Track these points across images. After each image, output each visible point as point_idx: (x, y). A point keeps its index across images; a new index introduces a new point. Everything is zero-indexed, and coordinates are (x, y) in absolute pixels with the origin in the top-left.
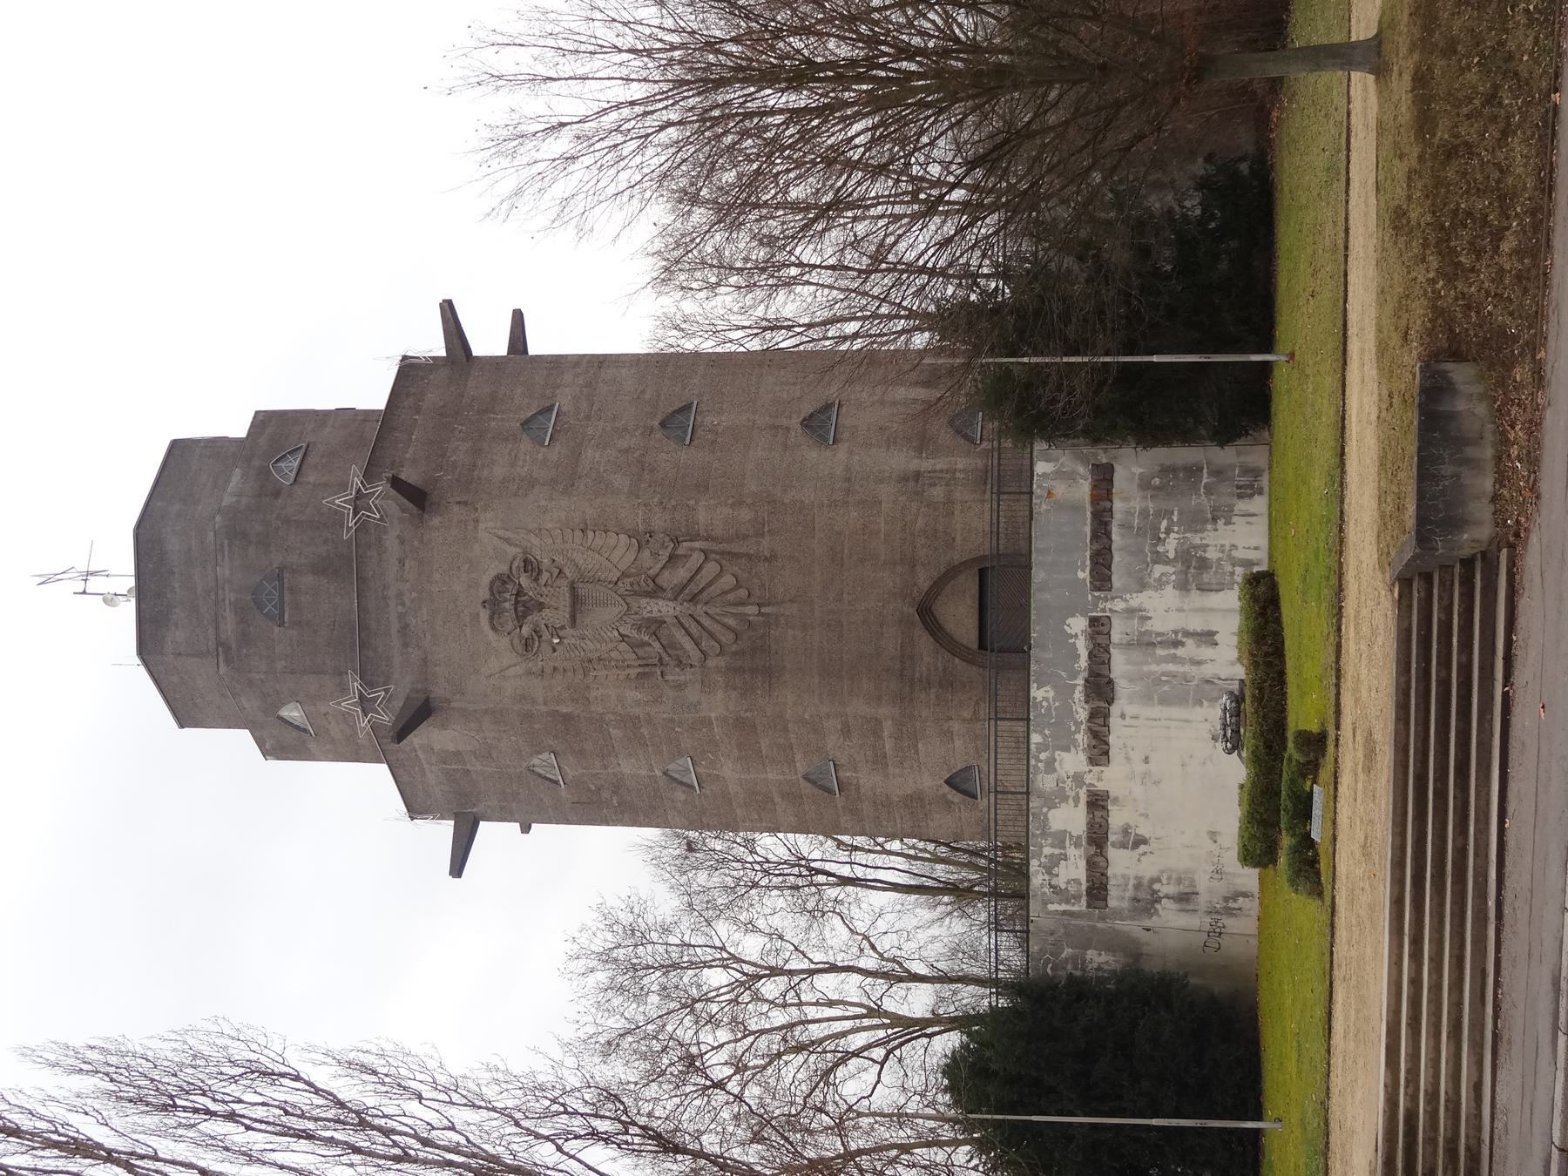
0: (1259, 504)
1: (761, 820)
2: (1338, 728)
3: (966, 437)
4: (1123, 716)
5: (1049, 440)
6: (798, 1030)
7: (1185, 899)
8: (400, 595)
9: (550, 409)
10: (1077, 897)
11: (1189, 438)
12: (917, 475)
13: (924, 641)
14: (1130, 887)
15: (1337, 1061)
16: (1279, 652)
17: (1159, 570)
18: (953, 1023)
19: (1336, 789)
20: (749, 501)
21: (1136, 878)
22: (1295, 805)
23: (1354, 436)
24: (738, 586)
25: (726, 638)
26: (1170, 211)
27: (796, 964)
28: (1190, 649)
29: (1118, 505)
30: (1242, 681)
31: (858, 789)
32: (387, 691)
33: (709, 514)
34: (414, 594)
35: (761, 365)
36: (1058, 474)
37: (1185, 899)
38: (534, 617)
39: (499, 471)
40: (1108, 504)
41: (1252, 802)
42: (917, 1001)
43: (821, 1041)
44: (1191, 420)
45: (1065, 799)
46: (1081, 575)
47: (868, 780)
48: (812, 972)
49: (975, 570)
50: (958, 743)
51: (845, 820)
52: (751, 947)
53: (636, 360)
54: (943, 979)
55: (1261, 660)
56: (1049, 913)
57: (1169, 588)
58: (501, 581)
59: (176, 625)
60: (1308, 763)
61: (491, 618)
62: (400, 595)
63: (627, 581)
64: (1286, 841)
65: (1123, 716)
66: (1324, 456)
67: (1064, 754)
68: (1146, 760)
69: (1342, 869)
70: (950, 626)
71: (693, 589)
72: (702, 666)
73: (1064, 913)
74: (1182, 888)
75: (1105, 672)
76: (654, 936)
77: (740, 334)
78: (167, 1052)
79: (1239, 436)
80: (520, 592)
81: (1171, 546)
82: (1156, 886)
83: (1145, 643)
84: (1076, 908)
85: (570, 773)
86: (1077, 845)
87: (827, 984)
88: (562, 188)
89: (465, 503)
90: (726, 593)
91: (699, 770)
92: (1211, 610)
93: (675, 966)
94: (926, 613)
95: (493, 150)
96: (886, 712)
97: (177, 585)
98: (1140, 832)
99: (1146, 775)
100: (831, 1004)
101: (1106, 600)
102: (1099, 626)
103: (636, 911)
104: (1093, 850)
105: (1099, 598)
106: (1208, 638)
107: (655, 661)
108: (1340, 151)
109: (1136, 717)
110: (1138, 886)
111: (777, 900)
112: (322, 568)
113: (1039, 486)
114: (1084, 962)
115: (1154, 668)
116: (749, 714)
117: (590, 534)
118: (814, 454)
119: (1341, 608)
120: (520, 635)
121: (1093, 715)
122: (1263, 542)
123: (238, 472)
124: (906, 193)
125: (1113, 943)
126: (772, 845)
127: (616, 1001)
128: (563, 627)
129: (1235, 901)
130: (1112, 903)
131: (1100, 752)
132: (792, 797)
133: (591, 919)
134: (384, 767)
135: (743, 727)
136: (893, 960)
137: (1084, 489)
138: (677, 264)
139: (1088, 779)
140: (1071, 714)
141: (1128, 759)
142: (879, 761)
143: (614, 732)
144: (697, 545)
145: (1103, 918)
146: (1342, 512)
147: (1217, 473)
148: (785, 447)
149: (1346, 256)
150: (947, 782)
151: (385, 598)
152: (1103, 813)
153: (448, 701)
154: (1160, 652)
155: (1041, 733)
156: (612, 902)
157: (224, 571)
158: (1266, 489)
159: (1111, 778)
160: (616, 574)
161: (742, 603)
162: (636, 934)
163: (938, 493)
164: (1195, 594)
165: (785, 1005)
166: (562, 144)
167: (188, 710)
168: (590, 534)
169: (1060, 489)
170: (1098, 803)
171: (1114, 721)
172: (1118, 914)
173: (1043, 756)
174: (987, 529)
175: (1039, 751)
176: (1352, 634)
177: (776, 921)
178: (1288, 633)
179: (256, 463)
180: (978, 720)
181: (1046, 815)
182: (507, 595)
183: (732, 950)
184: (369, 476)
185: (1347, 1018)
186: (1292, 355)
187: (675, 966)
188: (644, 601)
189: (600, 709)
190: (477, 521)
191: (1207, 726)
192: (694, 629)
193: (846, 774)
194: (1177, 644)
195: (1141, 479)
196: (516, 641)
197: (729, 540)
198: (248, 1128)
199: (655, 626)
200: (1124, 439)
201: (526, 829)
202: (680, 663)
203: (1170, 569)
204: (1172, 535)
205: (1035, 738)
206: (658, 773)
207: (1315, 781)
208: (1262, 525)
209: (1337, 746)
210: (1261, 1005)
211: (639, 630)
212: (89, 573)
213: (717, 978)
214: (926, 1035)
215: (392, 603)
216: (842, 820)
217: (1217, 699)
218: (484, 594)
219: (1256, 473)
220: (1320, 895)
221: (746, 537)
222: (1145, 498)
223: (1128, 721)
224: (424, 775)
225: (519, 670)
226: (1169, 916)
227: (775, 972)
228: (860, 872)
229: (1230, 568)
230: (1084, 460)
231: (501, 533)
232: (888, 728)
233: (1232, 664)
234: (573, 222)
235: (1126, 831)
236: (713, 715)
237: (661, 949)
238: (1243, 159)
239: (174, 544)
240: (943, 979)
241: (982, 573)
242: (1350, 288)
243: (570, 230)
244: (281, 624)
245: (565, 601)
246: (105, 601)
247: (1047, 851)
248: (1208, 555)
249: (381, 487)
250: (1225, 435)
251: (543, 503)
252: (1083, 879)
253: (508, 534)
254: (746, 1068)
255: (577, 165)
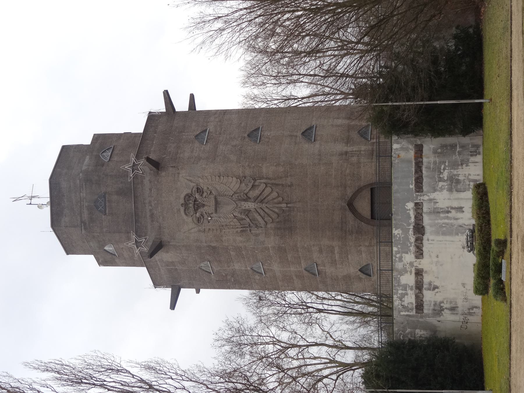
0: (479, 158)
1: (288, 286)
2: (511, 237)
3: (364, 138)
4: (428, 240)
5: (398, 135)
6: (303, 368)
7: (453, 309)
8: (150, 202)
9: (206, 131)
10: (412, 309)
11: (451, 133)
12: (346, 153)
13: (350, 216)
14: (432, 305)
15: (513, 362)
16: (488, 213)
17: (441, 184)
18: (361, 365)
19: (511, 260)
20: (282, 164)
21: (434, 301)
22: (495, 268)
23: (515, 126)
24: (278, 196)
25: (274, 216)
26: (443, 47)
27: (301, 343)
28: (453, 213)
29: (425, 160)
30: (474, 225)
31: (325, 273)
32: (146, 239)
33: (268, 169)
34: (155, 202)
35: (286, 112)
36: (402, 148)
37: (453, 309)
38: (201, 210)
39: (187, 155)
40: (421, 160)
41: (478, 270)
42: (349, 357)
43: (312, 372)
44: (452, 127)
45: (407, 272)
46: (411, 187)
47: (329, 270)
48: (308, 346)
49: (369, 189)
50: (364, 255)
51: (320, 286)
52: (285, 336)
53: (238, 112)
54: (360, 348)
55: (480, 216)
56: (401, 315)
57: (445, 191)
58: (188, 196)
59: (66, 216)
60: (500, 251)
61: (185, 210)
62: (150, 202)
63: (236, 195)
64: (492, 282)
65: (428, 240)
66: (504, 136)
67: (406, 255)
68: (437, 257)
69: (514, 290)
70: (360, 210)
71: (262, 197)
72: (266, 227)
73: (407, 315)
74: (452, 305)
75: (421, 223)
76: (247, 333)
77: (276, 102)
78: (78, 364)
79: (471, 132)
80: (196, 200)
81: (445, 175)
82: (442, 305)
83: (436, 212)
84: (411, 314)
85: (215, 269)
86: (411, 289)
87: (314, 351)
88: (218, 41)
89: (174, 167)
90: (274, 199)
91: (265, 267)
92: (462, 199)
93: (255, 344)
94: (351, 205)
95: (194, 27)
96: (336, 244)
97: (65, 200)
98: (435, 284)
99: (437, 262)
100: (315, 358)
101: (421, 196)
102: (418, 206)
103: (240, 323)
104: (417, 291)
105: (418, 195)
106: (460, 209)
107: (247, 226)
108: (508, 21)
109: (433, 240)
110: (435, 305)
111: (294, 319)
112: (121, 192)
113: (395, 153)
114: (415, 334)
115: (440, 221)
116: (283, 245)
117: (222, 177)
118: (307, 146)
119: (511, 192)
120: (196, 217)
121: (417, 240)
122: (481, 173)
123: (88, 157)
124: (339, 46)
125: (426, 326)
126: (292, 297)
127: (233, 357)
128: (212, 213)
129: (472, 309)
130: (425, 311)
131: (419, 254)
132: (300, 277)
133: (223, 325)
134: (144, 269)
135: (281, 250)
136: (339, 341)
137: (411, 154)
138: (253, 75)
139: (415, 264)
140: (408, 239)
141: (430, 256)
142: (334, 263)
143: (232, 253)
144: (262, 181)
145: (422, 317)
146: (511, 156)
147: (462, 147)
148: (296, 143)
149: (511, 60)
150: (360, 270)
151: (144, 203)
152: (421, 277)
153: (169, 242)
154: (442, 215)
155: (397, 247)
156: (231, 319)
157: (83, 195)
158: (482, 153)
159: (424, 264)
160: (231, 193)
161: (280, 203)
162: (240, 332)
163: (354, 159)
164: (455, 193)
165: (298, 359)
166: (219, 25)
167: (70, 249)
168: (222, 177)
169: (403, 154)
170: (419, 273)
171: (425, 242)
172: (428, 315)
173: (398, 256)
174: (373, 173)
175: (396, 254)
176: (516, 201)
177: (294, 327)
178: (492, 209)
179: (95, 153)
180: (371, 246)
181: (399, 278)
182: (191, 201)
183: (277, 338)
184: (138, 157)
185: (517, 345)
186: (491, 100)
187: (255, 344)
188: (243, 203)
189: (226, 244)
190: (179, 174)
191: (461, 243)
192: (262, 213)
193: (321, 268)
194: (448, 212)
195: (433, 150)
196: (194, 219)
197: (275, 179)
198: (109, 390)
199: (247, 212)
200: (427, 135)
201: (198, 292)
202: (257, 226)
203: (445, 184)
204: (446, 171)
205: (395, 249)
206: (249, 269)
207: (503, 258)
208: (480, 166)
209: (511, 244)
210: (483, 349)
211: (241, 214)
212: (32, 197)
213: (270, 348)
214: (352, 370)
215: (147, 205)
216: (319, 286)
217: (464, 233)
218: (182, 201)
219: (477, 146)
220: (506, 300)
221: (281, 178)
222: (435, 157)
223: (430, 242)
224: (160, 271)
225: (196, 230)
226: (448, 316)
227: (294, 346)
228: (326, 307)
229: (468, 183)
230: (411, 143)
231: (188, 178)
232: (337, 250)
233: (470, 219)
234: (224, 53)
235: (430, 284)
236: (270, 246)
237: (250, 338)
238: (471, 27)
239: (64, 185)
240: (360, 348)
241: (372, 190)
242: (513, 72)
243: (222, 57)
244: (105, 214)
245: (213, 203)
246: (38, 207)
247: (400, 292)
248: (459, 178)
249: (142, 161)
250: (466, 132)
251: (204, 166)
252: (414, 302)
253: (191, 178)
254: (283, 383)
255: (225, 32)
